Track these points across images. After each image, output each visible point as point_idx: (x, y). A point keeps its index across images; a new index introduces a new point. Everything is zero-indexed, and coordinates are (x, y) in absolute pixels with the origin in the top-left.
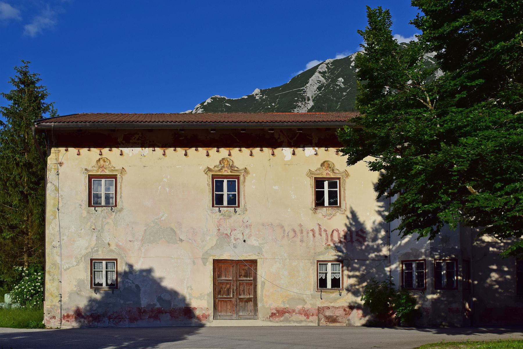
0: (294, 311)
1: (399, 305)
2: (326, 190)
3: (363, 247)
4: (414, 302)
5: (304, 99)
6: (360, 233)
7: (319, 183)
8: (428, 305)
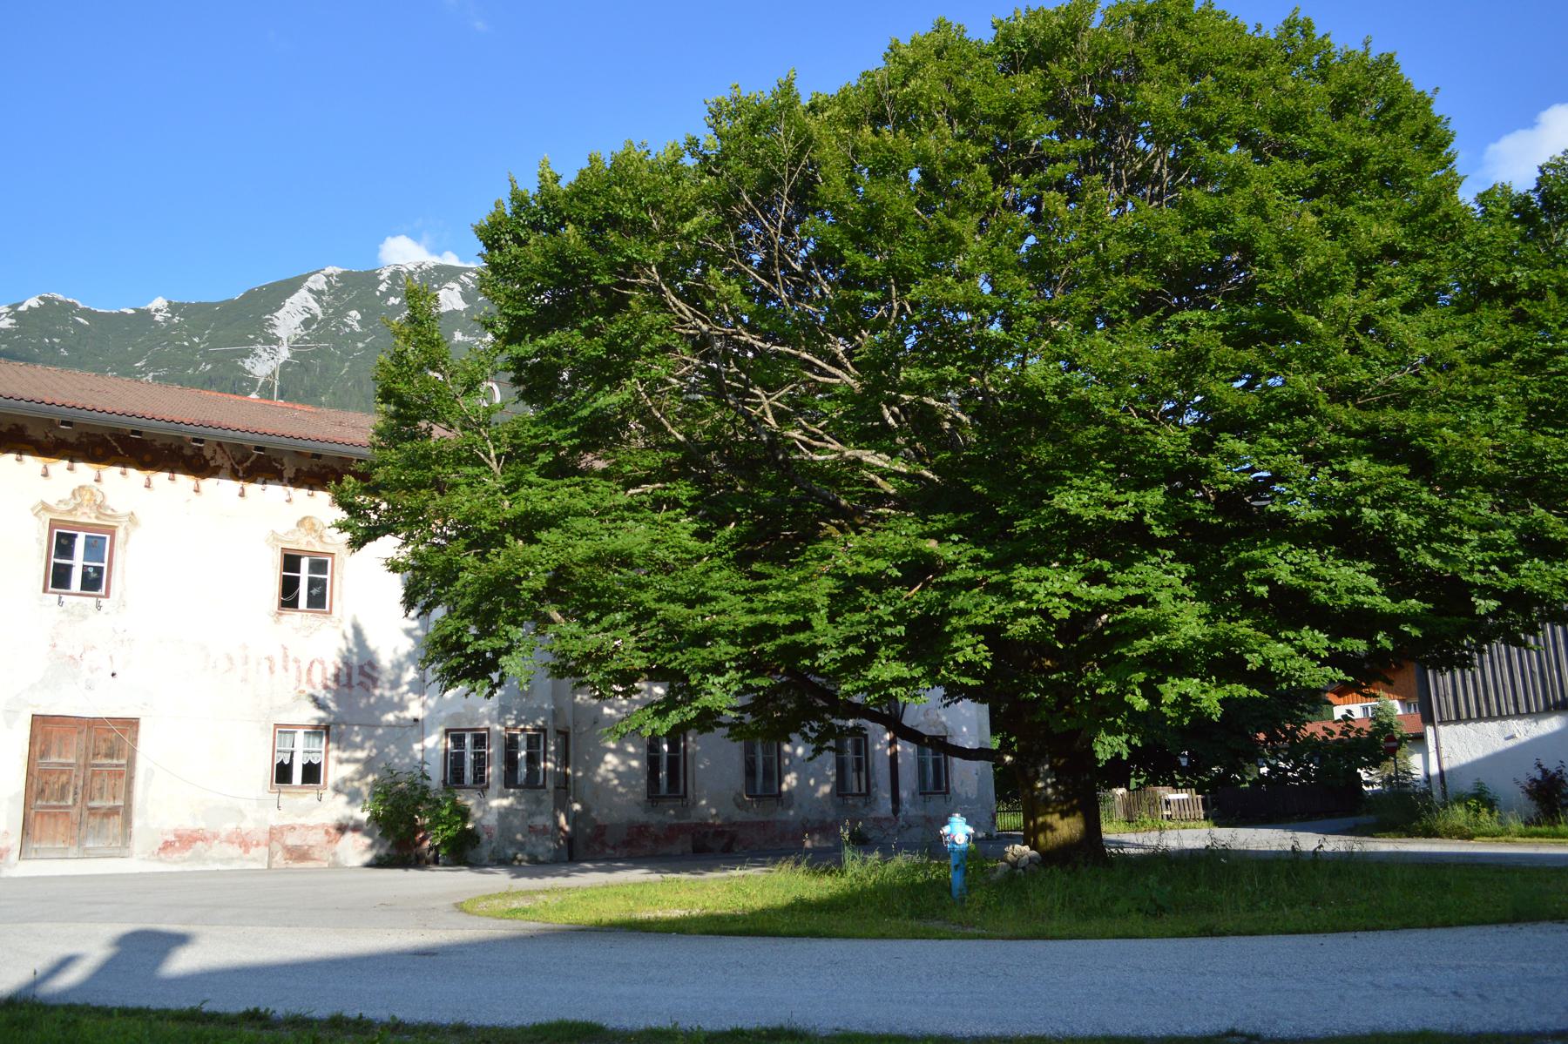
0: (216, 836)
1: (437, 820)
2: (304, 575)
3: (372, 700)
4: (465, 814)
5: (274, 341)
6: (367, 669)
7: (291, 562)
8: (491, 820)
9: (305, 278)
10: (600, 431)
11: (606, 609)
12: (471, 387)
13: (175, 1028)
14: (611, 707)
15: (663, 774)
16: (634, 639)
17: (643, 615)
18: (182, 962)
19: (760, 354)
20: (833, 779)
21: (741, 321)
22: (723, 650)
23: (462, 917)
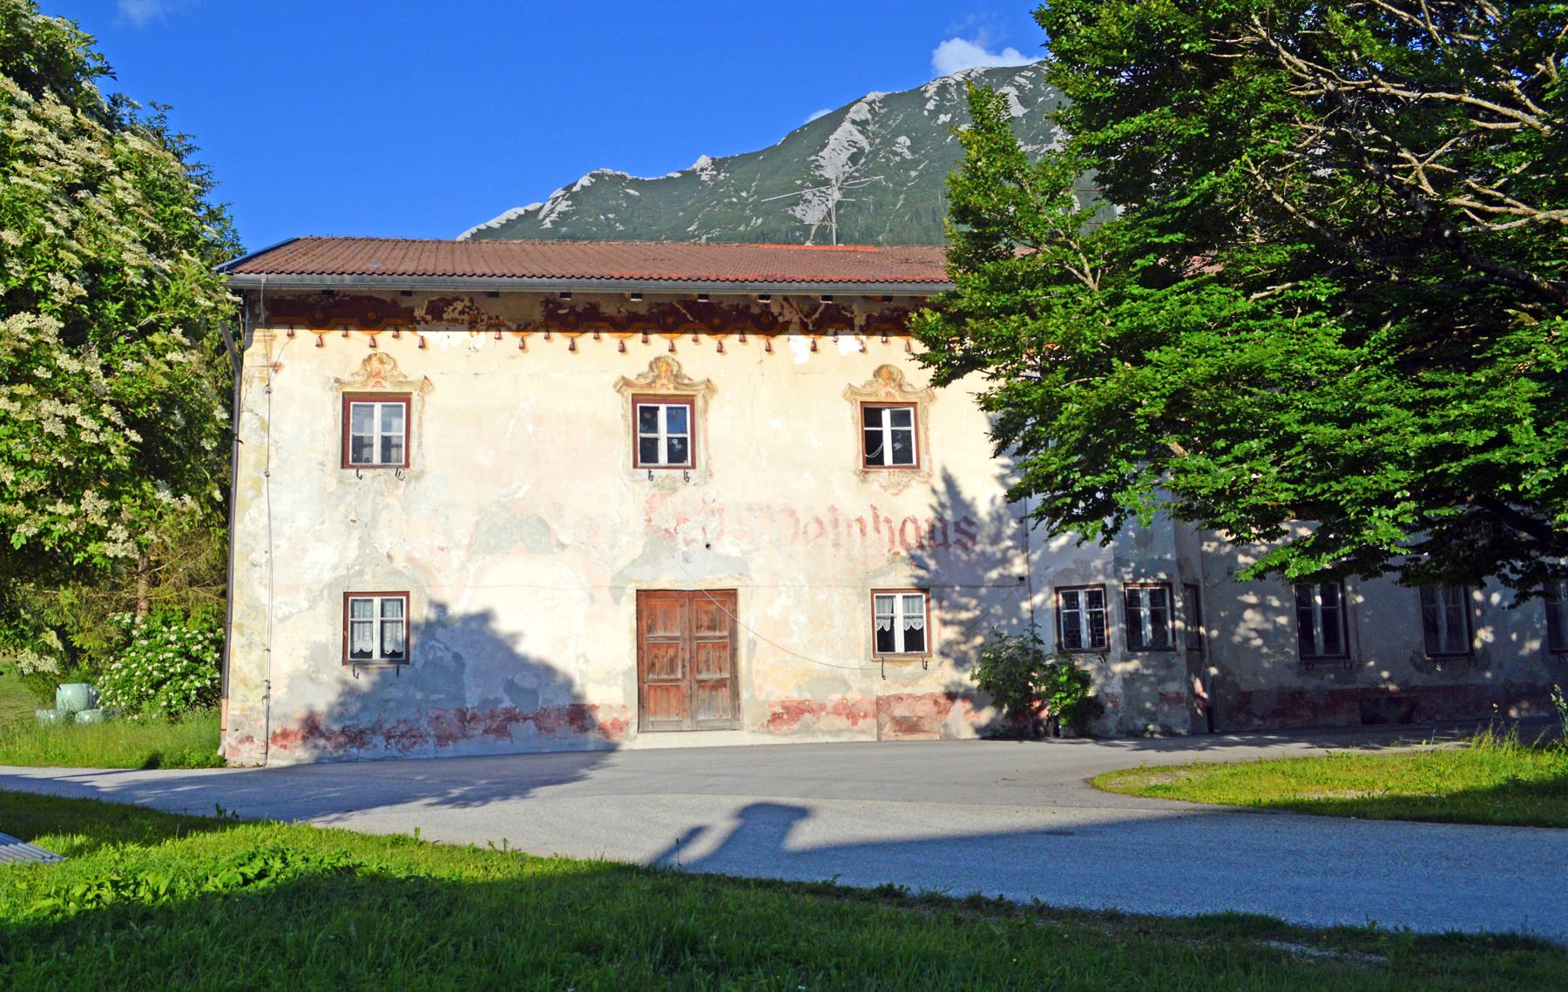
0: (822, 707)
1: (1055, 688)
2: (887, 428)
3: (973, 556)
6: (963, 526)
7: (871, 415)
9: (846, 109)
10: (1208, 227)
11: (1239, 436)
12: (1053, 193)
13: (811, 901)
14: (1247, 554)
15: (1318, 630)
16: (1276, 469)
17: (1283, 442)
18: (804, 836)
19: (1403, 106)
20: (1544, 633)
21: (1375, 70)
22: (1391, 477)
23: (1093, 795)
